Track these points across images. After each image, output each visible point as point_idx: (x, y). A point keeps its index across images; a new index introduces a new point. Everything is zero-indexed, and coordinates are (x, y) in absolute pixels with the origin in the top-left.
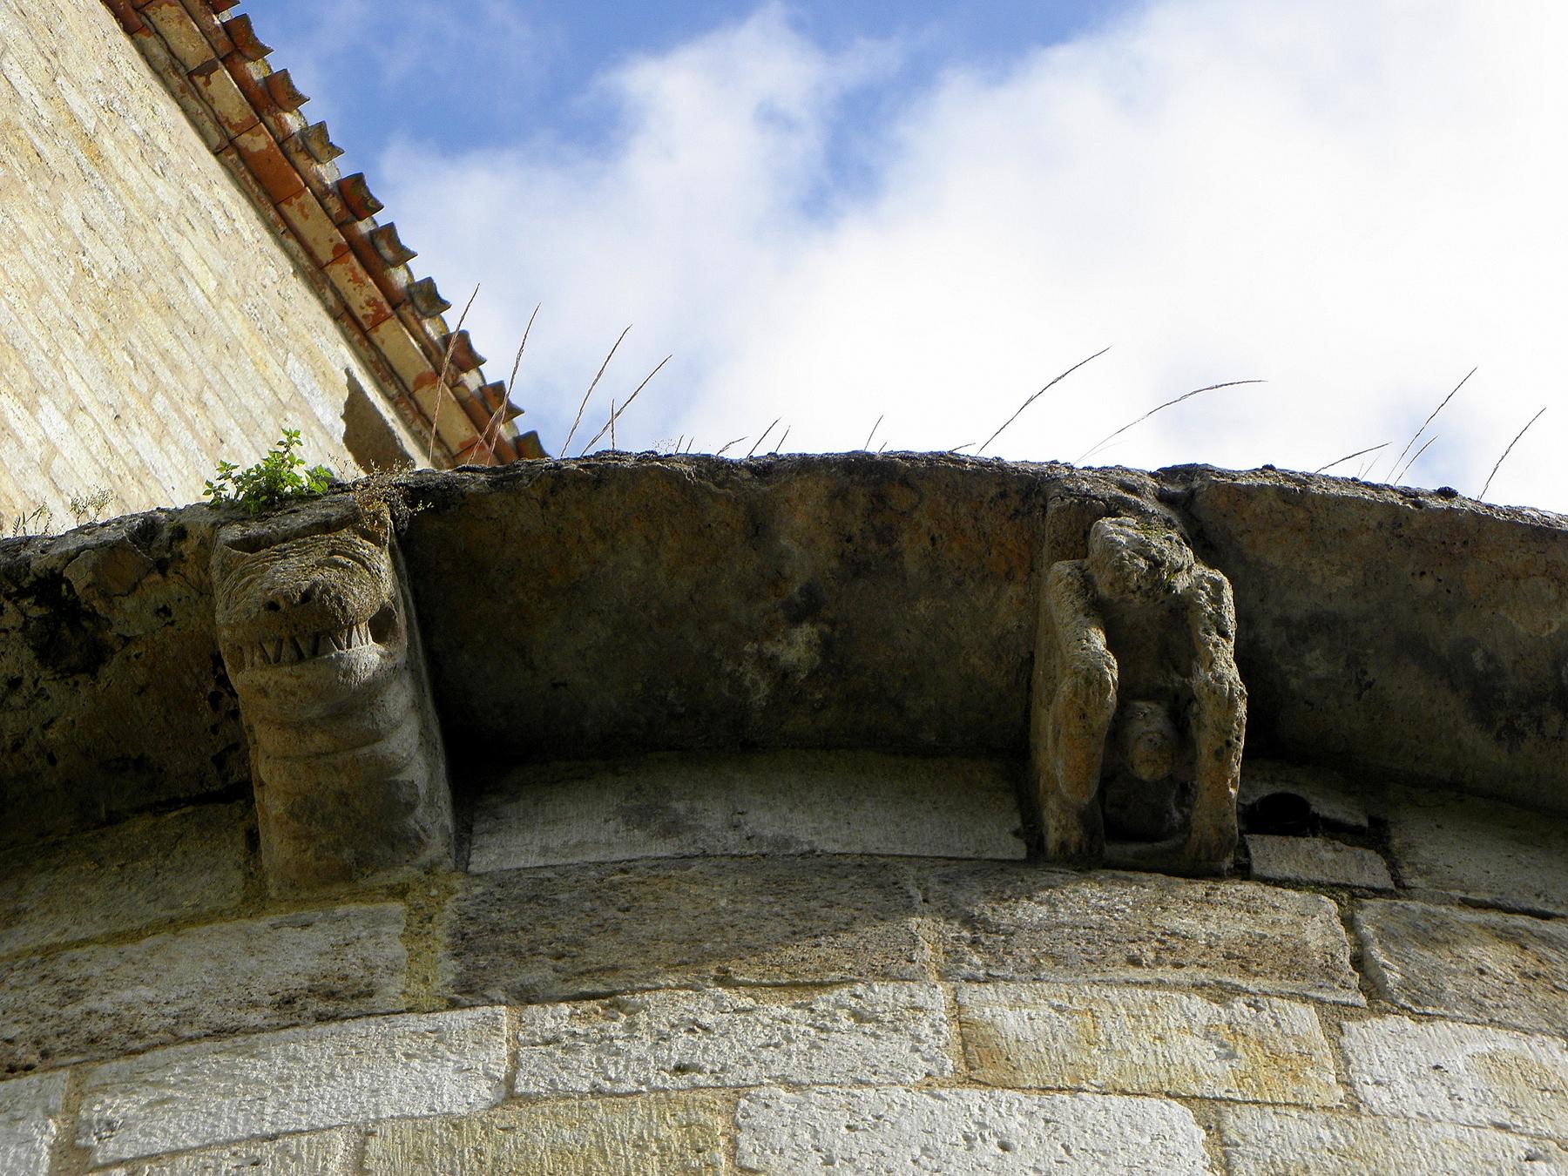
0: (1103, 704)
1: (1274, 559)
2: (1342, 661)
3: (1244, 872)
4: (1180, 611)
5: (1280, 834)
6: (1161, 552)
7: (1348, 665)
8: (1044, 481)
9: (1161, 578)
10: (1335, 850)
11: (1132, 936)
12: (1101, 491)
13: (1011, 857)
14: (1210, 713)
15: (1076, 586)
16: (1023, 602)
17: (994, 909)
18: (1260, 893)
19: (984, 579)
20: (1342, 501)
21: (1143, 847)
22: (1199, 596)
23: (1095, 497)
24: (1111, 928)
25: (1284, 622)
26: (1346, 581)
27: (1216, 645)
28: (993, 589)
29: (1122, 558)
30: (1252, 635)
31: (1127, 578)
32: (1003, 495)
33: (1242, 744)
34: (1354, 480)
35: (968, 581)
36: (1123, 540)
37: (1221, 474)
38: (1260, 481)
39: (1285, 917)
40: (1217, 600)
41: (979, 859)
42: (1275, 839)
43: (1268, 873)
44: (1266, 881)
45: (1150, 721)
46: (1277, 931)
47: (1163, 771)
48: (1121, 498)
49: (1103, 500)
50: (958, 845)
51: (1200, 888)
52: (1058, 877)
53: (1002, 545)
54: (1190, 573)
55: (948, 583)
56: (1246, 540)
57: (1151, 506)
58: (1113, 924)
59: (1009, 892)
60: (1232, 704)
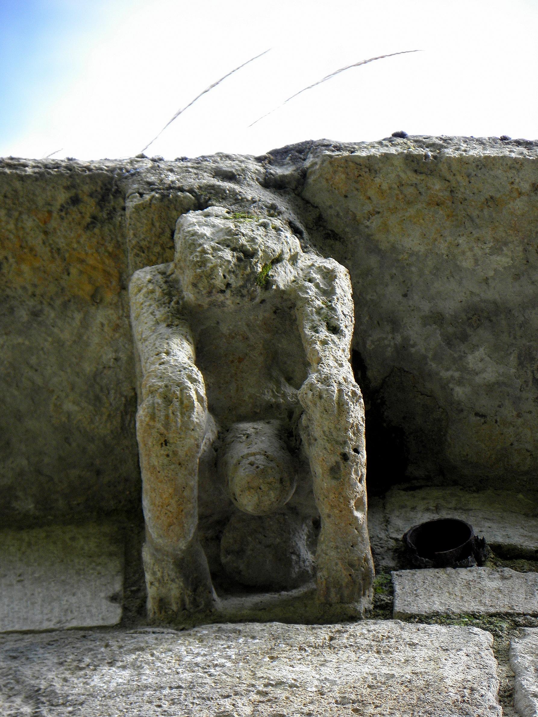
0: (187, 427)
1: (412, 242)
2: (513, 359)
3: (384, 610)
4: (286, 310)
5: (436, 566)
6: (253, 240)
7: (521, 364)
8: (122, 177)
9: (253, 272)
10: (503, 578)
11: (228, 691)
12: (192, 182)
13: (101, 623)
14: (317, 424)
15: (158, 293)
16: (116, 328)
17: (65, 680)
18: (398, 631)
19: (65, 305)
20: (484, 164)
21: (267, 597)
22: (304, 290)
23: (181, 189)
24: (202, 685)
25: (437, 318)
26: (502, 261)
27: (324, 343)
28: (78, 316)
29: (204, 252)
30: (399, 339)
31: (211, 275)
32: (75, 201)
33: (363, 457)
34: (504, 139)
35: (47, 309)
36: (207, 231)
37: (338, 148)
38: (384, 150)
39: (422, 653)
40: (328, 293)
41: (60, 630)
42: (430, 573)
43: (413, 609)
44: (409, 618)
45: (256, 440)
46: (409, 669)
47: (270, 498)
48: (213, 187)
49: (191, 191)
50: (38, 617)
51: (324, 632)
52: (150, 638)
53: (82, 261)
54: (297, 265)
55: (23, 315)
56: (375, 223)
57: (252, 191)
58: (209, 680)
59: (87, 660)
60: (342, 408)
